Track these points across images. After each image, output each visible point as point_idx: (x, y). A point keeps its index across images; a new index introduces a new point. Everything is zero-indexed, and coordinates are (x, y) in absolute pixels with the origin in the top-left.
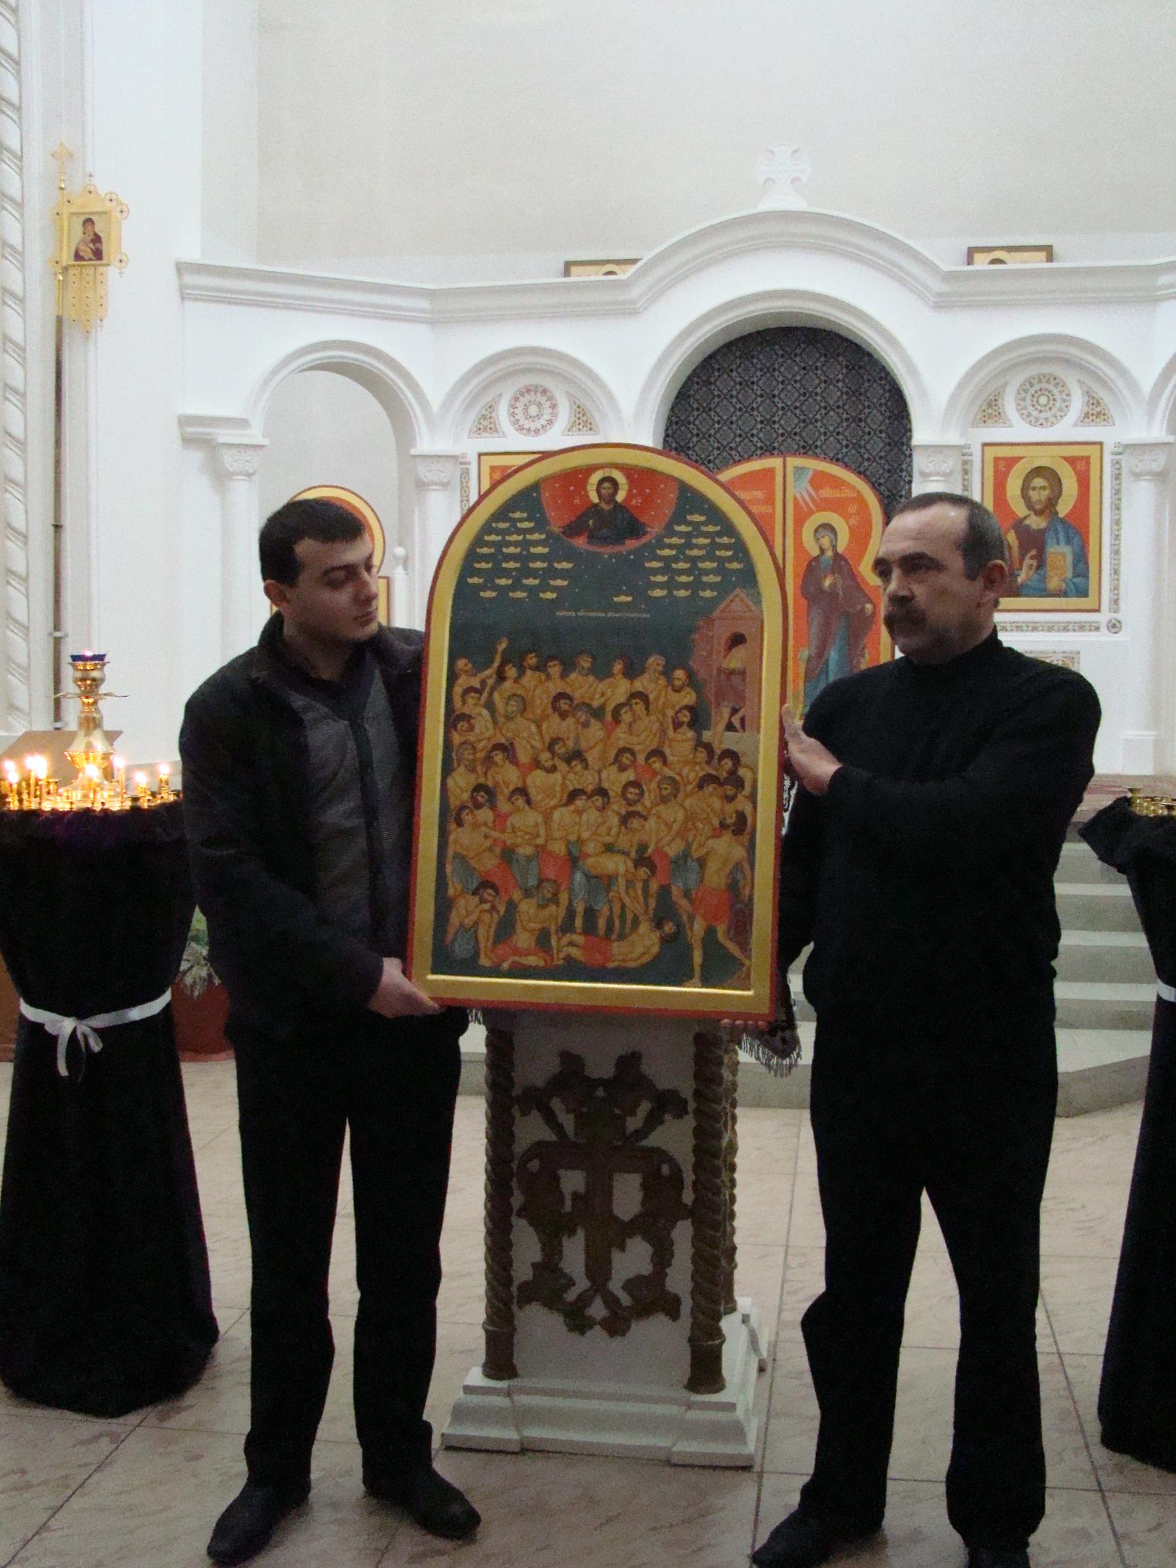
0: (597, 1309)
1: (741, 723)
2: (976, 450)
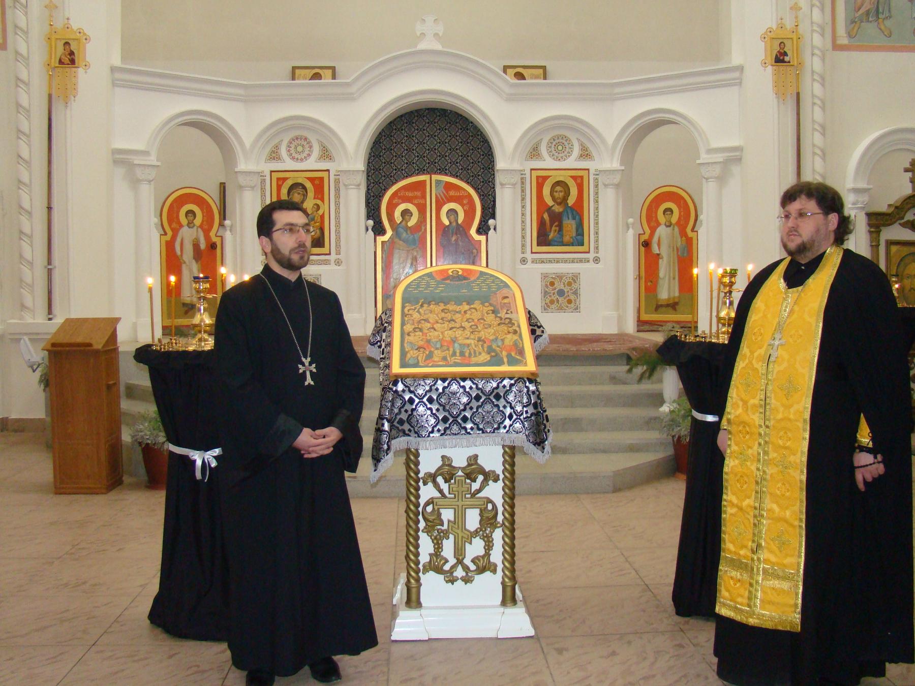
0: (459, 572)
1: (509, 308)
2: (528, 172)
